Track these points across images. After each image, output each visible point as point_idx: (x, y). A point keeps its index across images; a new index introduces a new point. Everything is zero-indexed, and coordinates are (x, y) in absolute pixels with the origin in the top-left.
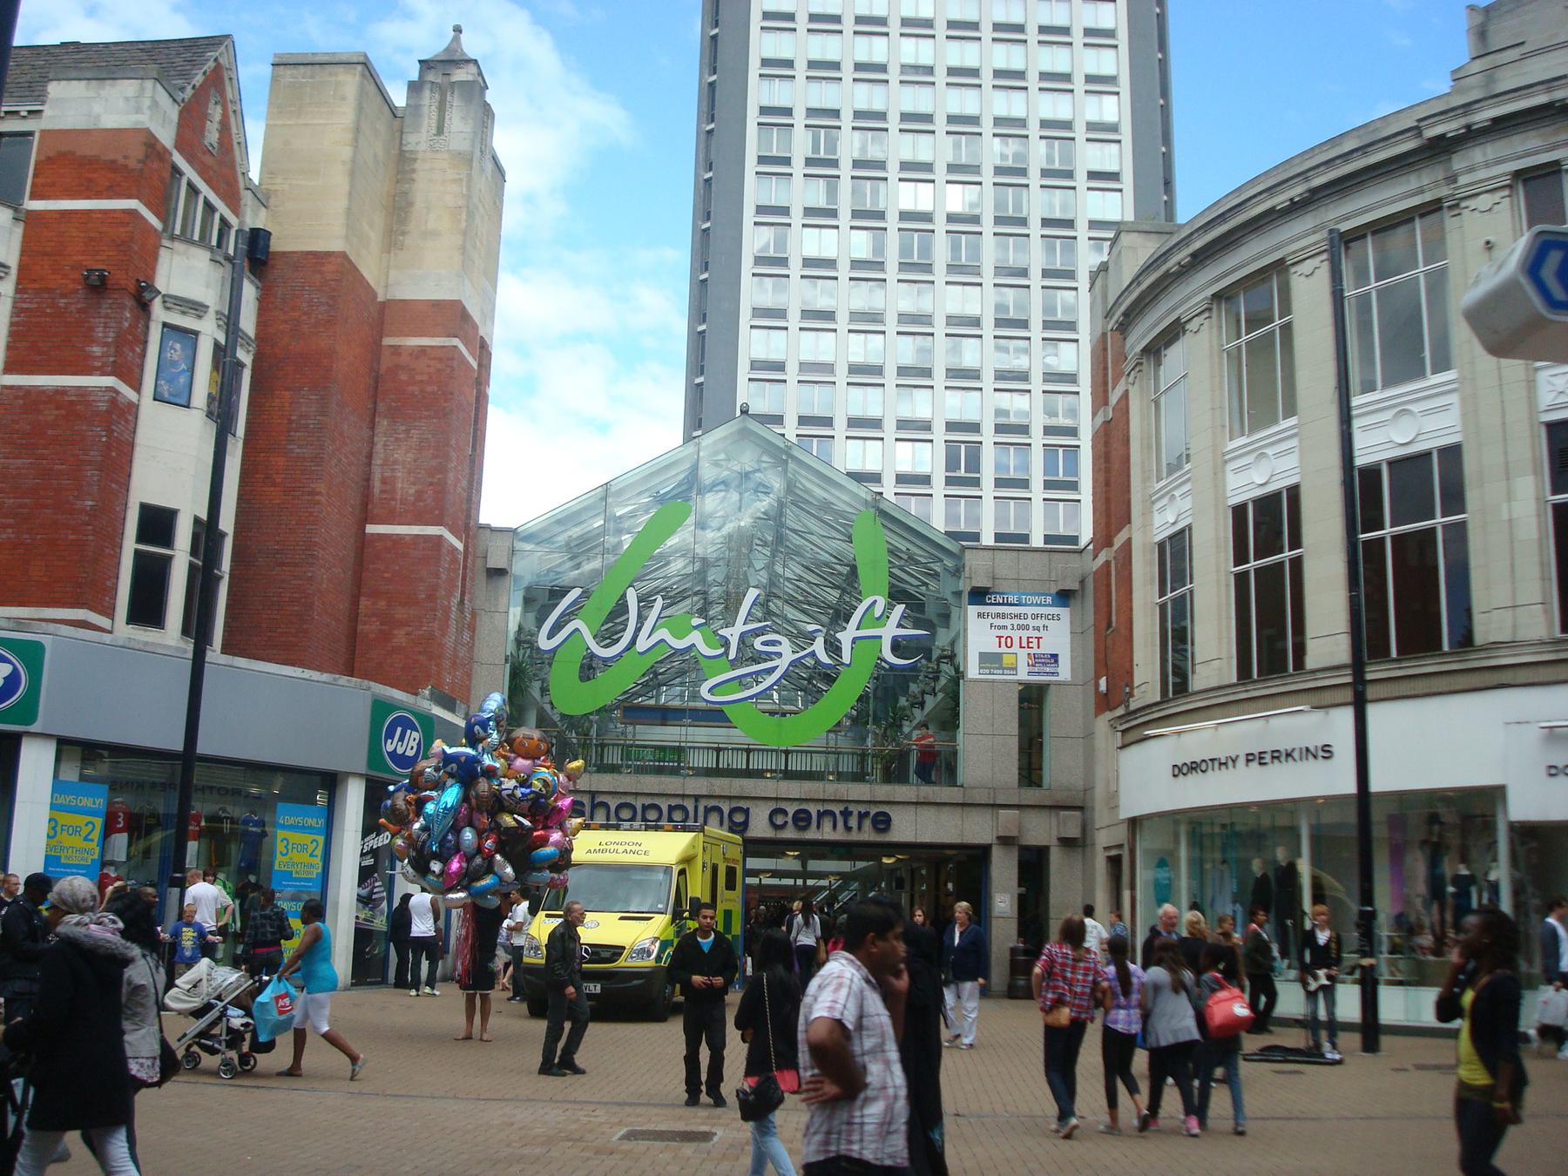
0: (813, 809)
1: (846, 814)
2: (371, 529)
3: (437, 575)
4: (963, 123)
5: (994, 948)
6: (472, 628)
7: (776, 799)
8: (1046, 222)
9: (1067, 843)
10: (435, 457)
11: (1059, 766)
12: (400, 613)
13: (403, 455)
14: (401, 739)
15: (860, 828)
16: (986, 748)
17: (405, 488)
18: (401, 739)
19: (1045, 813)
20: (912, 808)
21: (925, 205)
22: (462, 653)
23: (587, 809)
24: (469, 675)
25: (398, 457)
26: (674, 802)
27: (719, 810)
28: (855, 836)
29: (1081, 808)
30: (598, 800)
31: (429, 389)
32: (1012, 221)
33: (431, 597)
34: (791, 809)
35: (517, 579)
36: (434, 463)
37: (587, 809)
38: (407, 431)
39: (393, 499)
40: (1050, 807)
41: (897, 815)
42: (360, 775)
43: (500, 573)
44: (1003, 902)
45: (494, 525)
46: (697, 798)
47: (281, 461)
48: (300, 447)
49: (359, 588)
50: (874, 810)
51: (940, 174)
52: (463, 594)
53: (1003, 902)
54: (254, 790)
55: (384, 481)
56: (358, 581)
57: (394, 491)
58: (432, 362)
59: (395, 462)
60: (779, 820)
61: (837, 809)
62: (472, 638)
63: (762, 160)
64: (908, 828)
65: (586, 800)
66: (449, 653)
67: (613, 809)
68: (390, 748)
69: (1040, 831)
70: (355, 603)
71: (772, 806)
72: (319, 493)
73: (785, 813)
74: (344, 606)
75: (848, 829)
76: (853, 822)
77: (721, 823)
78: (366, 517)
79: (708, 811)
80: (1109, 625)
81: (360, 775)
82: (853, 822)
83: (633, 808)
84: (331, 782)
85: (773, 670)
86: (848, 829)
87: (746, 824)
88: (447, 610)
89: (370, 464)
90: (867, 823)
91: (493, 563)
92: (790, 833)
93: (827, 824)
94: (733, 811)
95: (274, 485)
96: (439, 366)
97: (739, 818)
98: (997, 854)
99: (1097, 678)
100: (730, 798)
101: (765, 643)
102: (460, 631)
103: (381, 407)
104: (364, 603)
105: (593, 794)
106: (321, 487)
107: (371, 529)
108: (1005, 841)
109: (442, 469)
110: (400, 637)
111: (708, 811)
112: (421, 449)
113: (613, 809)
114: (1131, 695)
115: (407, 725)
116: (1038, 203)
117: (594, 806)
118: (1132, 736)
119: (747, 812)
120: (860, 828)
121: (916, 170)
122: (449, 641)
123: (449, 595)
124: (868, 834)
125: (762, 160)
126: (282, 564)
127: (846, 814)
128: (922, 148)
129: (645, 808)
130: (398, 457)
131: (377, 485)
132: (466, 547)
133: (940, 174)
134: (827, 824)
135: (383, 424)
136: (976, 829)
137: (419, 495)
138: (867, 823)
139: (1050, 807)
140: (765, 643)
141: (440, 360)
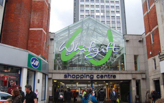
0: (104, 75)
1: (109, 75)
2: (30, 29)
3: (41, 36)
4: (102, 6)
5: (133, 96)
6: (48, 47)
7: (98, 73)
8: (112, 17)
9: (143, 79)
10: (41, 17)
11: (141, 67)
12: (35, 42)
13: (36, 17)
14: (35, 62)
15: (111, 77)
16: (129, 64)
17: (36, 22)
18: (35, 62)
19: (139, 74)
20: (119, 74)
21: (99, 15)
22: (46, 51)
23: (67, 76)
24: (48, 55)
25: (35, 18)
26: (81, 74)
27: (89, 75)
28: (110, 79)
29: (145, 74)
30: (69, 74)
31: (40, 7)
32: (108, 17)
33: (41, 40)
34: (100, 75)
35: (55, 41)
36: (41, 18)
37: (67, 76)
38: (37, 14)
39: (34, 24)
40: (140, 74)
41: (117, 75)
42: (26, 68)
43: (52, 39)
44: (134, 88)
45: (51, 32)
46: (85, 74)
47: (13, 15)
48: (17, 12)
49: (28, 39)
50: (113, 75)
51: (100, 12)
52: (46, 41)
53: (134, 88)
54: (6, 71)
55: (33, 22)
56: (28, 37)
57: (34, 23)
58: (40, 3)
59: (35, 18)
60: (98, 77)
61: (107, 75)
62: (48, 49)
63: (81, 10)
64: (118, 77)
65: (67, 74)
66: (44, 50)
67: (71, 76)
68: (32, 63)
69: (139, 77)
70: (28, 41)
71: (97, 74)
72: (20, 20)
73: (99, 76)
74: (25, 41)
75: (109, 78)
76: (110, 77)
77: (89, 78)
78: (30, 27)
79: (87, 76)
80: (151, 44)
81: (26, 68)
82: (110, 77)
83: (75, 75)
84: (21, 69)
85: (95, 54)
86: (109, 78)
87: (93, 78)
88: (44, 43)
89: (30, 19)
90: (112, 77)
91: (51, 38)
92: (100, 79)
93: (106, 77)
94: (91, 76)
95: (12, 19)
96: (42, 4)
97: (92, 77)
98: (132, 81)
99: (68, 87)
100: (90, 73)
101: (94, 49)
102: (46, 47)
103: (32, 10)
104: (29, 41)
105: (68, 73)
106: (20, 19)
107: (30, 29)
108: (134, 79)
109: (42, 19)
110: (35, 46)
111: (87, 76)
112: (39, 16)
113: (71, 76)
114: (161, 52)
115: (36, 60)
116: (111, 15)
117: (69, 75)
118: (162, 59)
119: (93, 76)
120: (111, 77)
121: (98, 11)
122: (44, 48)
123: (44, 40)
124: (112, 79)
125: (81, 10)
126: (13, 32)
127: (109, 75)
128: (98, 9)
129: (77, 75)
130: (35, 18)
131: (31, 22)
132: (47, 34)
133: (100, 12)
134: (106, 77)
135: (32, 13)
136: (129, 77)
137: (38, 24)
138: (112, 77)
139: (140, 74)
140: (94, 49)
141: (42, 3)
